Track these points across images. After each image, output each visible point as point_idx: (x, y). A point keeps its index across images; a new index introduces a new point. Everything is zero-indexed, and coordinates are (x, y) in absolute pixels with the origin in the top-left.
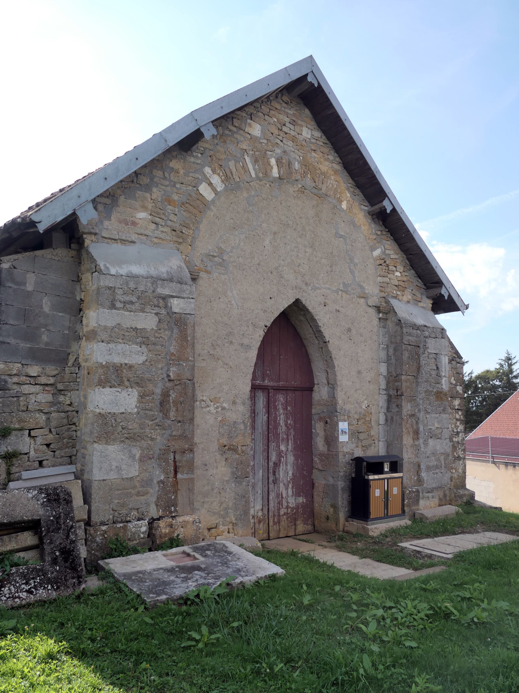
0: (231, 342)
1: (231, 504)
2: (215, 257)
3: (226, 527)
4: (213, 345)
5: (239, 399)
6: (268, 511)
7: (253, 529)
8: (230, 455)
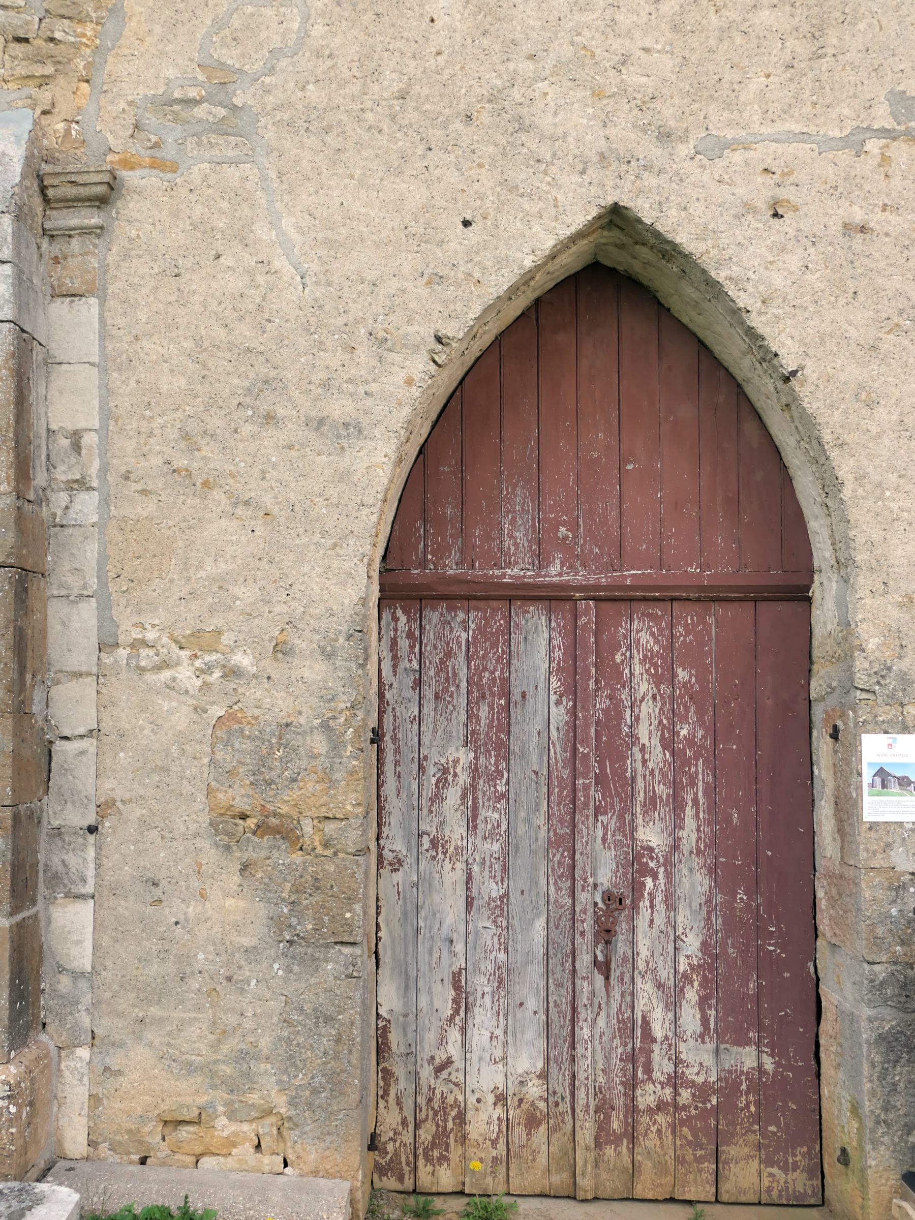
0: (270, 418)
1: (265, 1043)
2: (195, 102)
3: (245, 1127)
4: (186, 437)
5: (307, 634)
6: (573, 1086)
7: (502, 1146)
8: (263, 854)
